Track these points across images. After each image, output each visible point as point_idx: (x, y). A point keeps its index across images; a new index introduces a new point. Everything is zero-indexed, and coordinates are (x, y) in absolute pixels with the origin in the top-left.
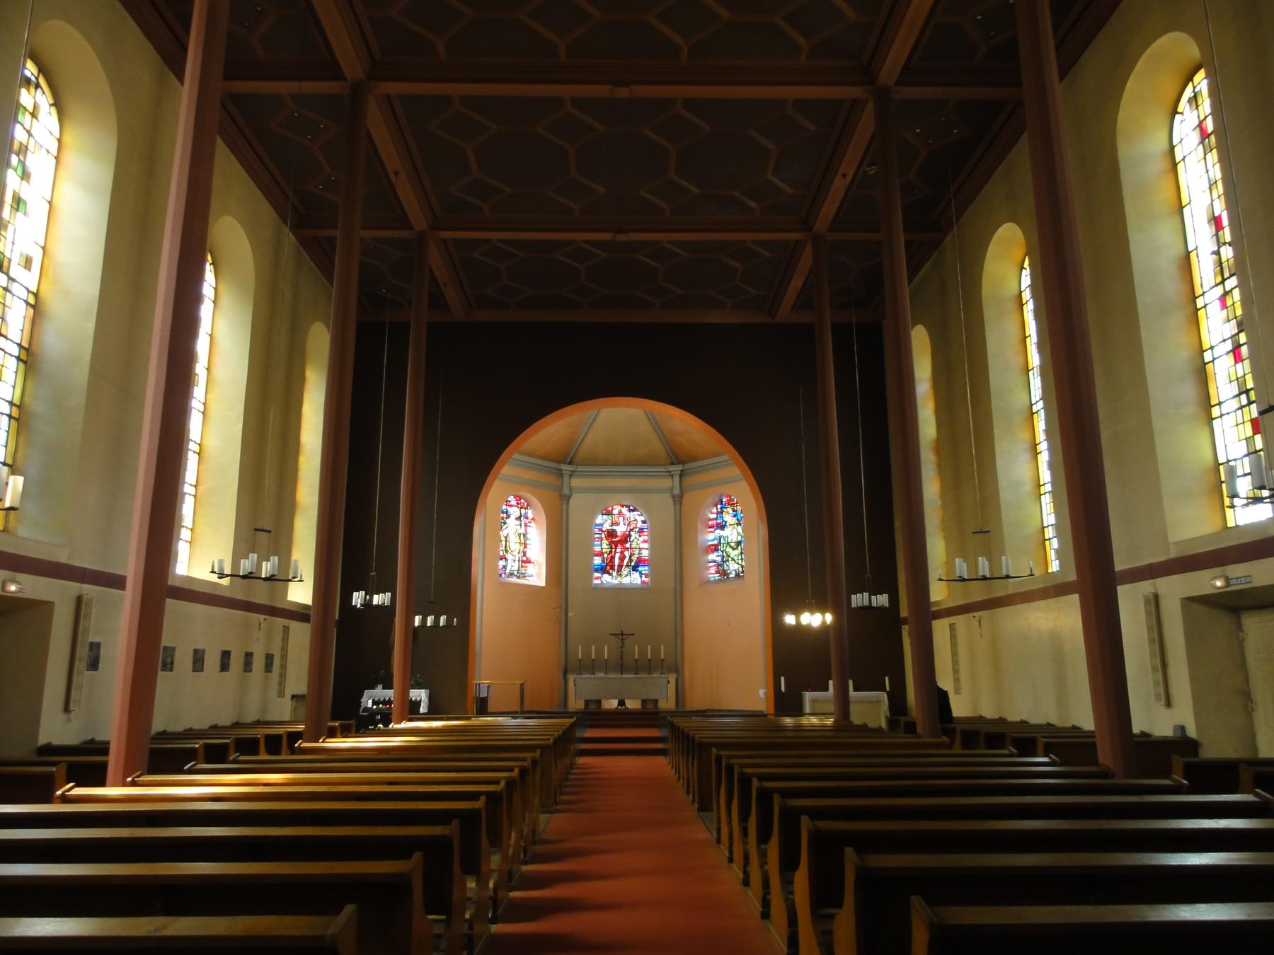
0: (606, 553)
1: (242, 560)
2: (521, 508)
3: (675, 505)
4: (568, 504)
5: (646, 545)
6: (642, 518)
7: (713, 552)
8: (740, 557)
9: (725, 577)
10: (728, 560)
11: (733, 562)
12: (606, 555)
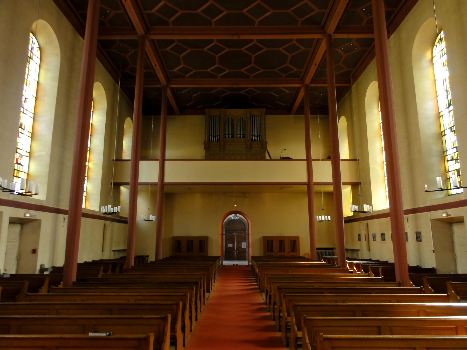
1: (102, 207)
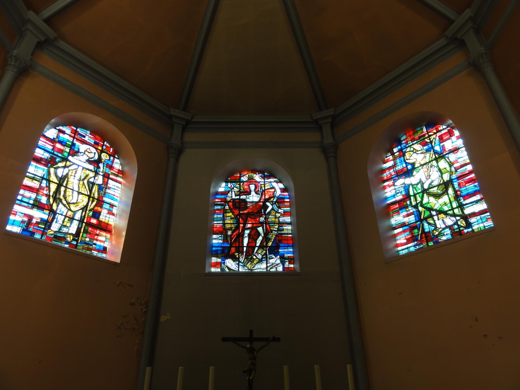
0: (230, 229)
2: (102, 151)
3: (327, 159)
4: (177, 160)
5: (288, 219)
6: (281, 186)
7: (398, 213)
8: (455, 205)
9: (431, 244)
10: (431, 216)
11: (442, 216)
12: (229, 233)
